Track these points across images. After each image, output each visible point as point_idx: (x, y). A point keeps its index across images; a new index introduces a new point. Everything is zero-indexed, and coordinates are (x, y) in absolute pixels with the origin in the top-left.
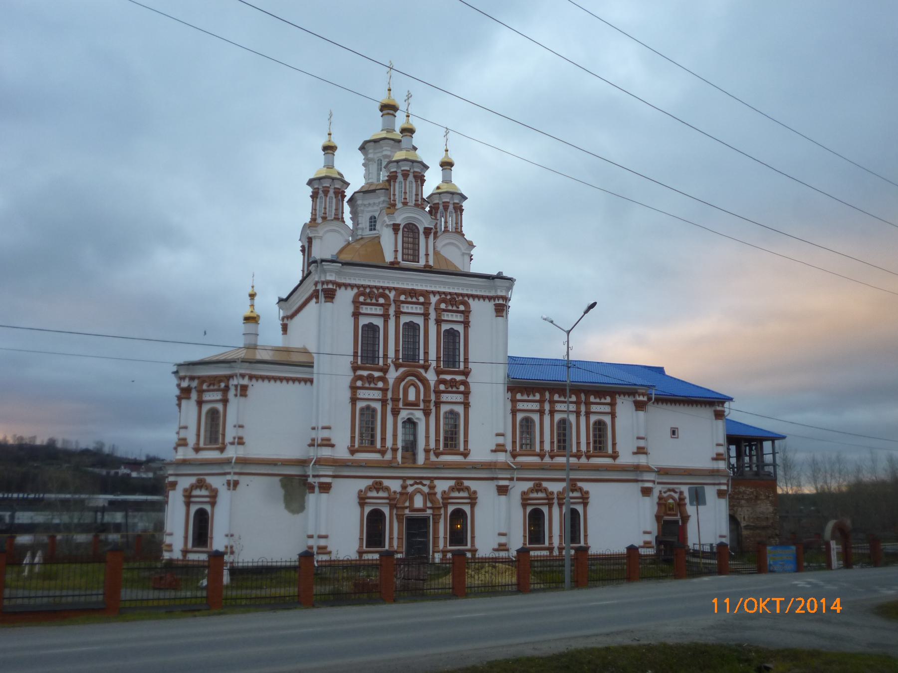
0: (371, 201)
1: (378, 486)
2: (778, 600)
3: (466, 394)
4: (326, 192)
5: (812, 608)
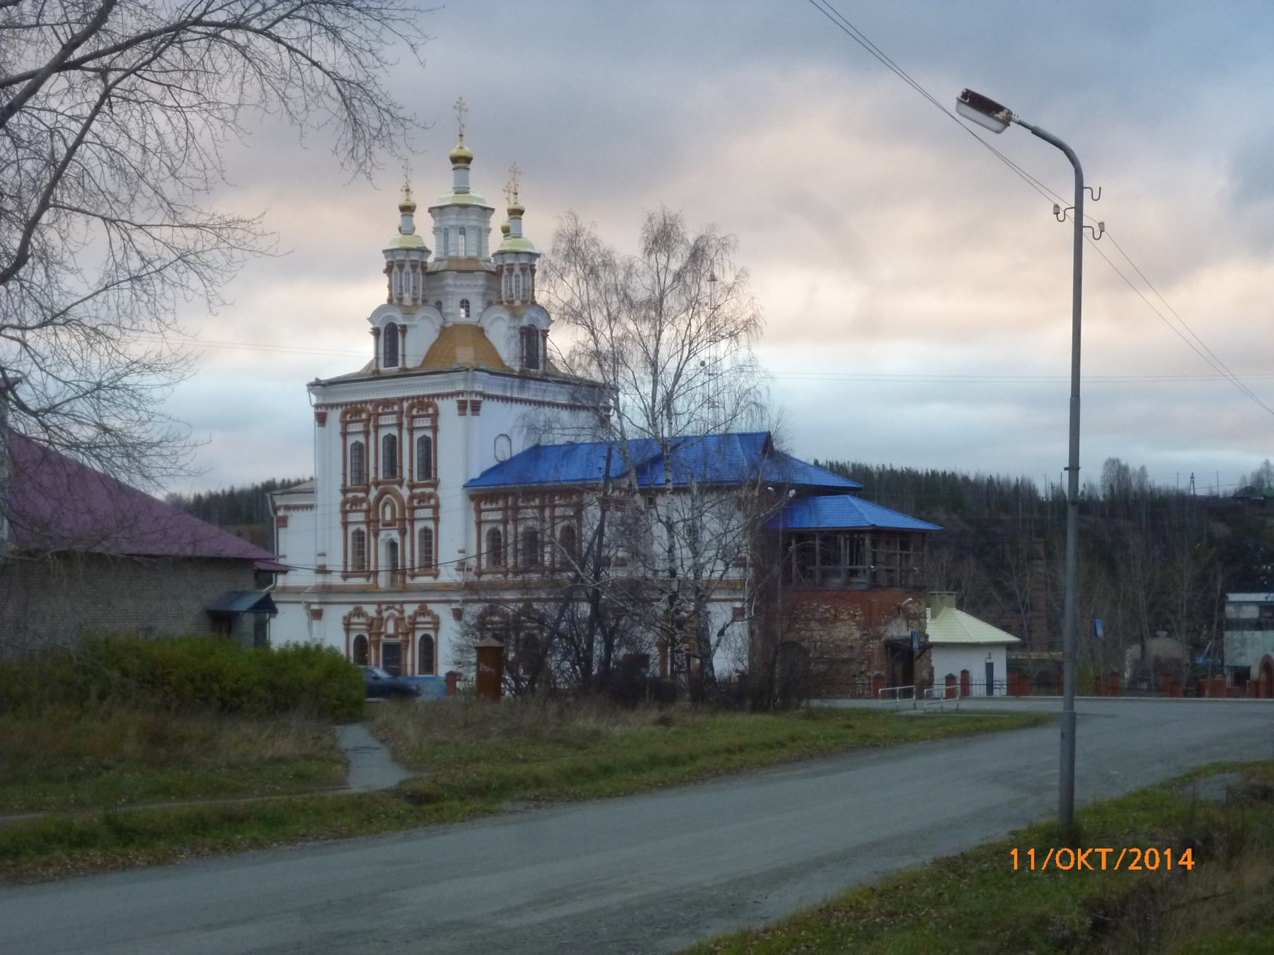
0: (465, 283)
1: (358, 613)
2: (1104, 851)
3: (436, 508)
4: (401, 267)
5: (1152, 862)
